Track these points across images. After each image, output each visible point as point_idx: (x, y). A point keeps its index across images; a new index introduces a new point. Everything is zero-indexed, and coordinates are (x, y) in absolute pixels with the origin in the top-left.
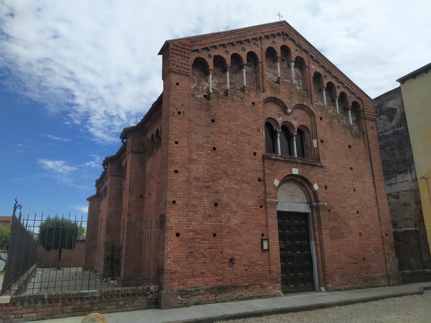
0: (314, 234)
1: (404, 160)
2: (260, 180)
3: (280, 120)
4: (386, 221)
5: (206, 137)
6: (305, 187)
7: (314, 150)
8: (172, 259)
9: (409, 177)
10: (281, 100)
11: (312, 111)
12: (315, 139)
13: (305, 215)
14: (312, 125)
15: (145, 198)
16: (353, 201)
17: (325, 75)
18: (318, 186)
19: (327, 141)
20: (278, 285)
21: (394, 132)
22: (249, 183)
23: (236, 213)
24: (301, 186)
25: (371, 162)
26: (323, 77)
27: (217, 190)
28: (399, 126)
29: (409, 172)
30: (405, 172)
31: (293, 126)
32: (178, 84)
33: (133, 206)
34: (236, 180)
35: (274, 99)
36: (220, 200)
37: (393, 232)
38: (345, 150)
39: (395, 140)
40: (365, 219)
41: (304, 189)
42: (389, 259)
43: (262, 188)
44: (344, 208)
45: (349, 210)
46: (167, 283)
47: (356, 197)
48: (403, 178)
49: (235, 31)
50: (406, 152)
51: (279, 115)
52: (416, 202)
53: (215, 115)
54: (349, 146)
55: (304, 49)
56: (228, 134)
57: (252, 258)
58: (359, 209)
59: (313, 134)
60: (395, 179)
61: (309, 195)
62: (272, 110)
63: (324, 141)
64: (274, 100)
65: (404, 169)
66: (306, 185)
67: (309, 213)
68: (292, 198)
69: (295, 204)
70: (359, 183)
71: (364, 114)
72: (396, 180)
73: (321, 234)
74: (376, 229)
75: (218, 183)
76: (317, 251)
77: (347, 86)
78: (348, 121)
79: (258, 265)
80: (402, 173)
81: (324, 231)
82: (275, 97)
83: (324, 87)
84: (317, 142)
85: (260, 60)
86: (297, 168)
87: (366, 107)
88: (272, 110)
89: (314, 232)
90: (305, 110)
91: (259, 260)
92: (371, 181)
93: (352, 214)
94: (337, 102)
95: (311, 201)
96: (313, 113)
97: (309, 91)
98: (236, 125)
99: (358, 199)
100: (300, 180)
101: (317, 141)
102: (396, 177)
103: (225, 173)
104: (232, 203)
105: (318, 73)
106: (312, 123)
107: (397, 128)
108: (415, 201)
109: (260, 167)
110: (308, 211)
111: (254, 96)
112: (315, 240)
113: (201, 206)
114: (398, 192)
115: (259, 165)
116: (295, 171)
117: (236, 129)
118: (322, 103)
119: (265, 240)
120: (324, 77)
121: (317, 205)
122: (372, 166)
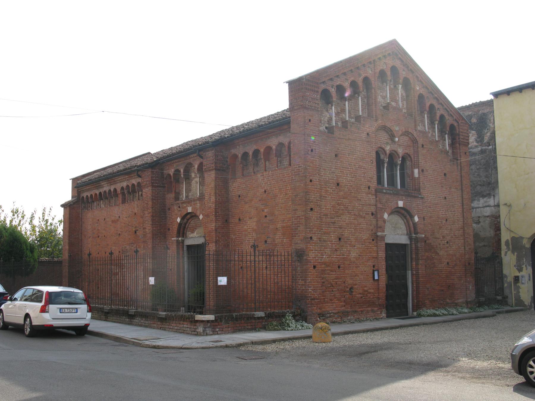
0: (412, 264)
1: (489, 184)
2: (372, 214)
3: (388, 148)
4: (470, 251)
5: (332, 173)
6: (406, 219)
7: (415, 180)
8: (312, 288)
9: (491, 202)
10: (389, 128)
11: (416, 138)
12: (417, 168)
13: (405, 245)
14: (414, 153)
15: (229, 223)
17: (428, 97)
18: (418, 218)
20: (384, 310)
21: (482, 150)
22: (364, 218)
23: (355, 246)
24: (403, 218)
25: (462, 191)
26: (426, 99)
28: (488, 144)
29: (492, 197)
30: (489, 195)
31: (398, 155)
32: (310, 121)
33: (220, 232)
34: (354, 215)
35: (384, 127)
36: (343, 235)
37: (431, 244)
38: (441, 179)
39: (481, 159)
40: (453, 248)
41: (405, 221)
42: (469, 287)
43: (374, 222)
44: (437, 238)
45: (441, 241)
46: (310, 307)
47: (447, 228)
48: (486, 202)
50: (491, 175)
51: (387, 143)
52: (496, 229)
53: (338, 149)
54: (445, 174)
55: (411, 69)
56: (348, 168)
57: (366, 287)
58: (449, 239)
59: (415, 162)
60: (478, 203)
61: (409, 226)
62: (381, 139)
63: (425, 170)
64: (385, 128)
65: (488, 192)
66: (408, 217)
67: (407, 244)
69: (397, 236)
70: (451, 213)
71: (459, 139)
72: (478, 204)
73: (417, 264)
74: (461, 258)
76: (412, 281)
77: (447, 108)
78: (444, 145)
79: (370, 293)
80: (485, 197)
81: (421, 262)
83: (426, 110)
84: (419, 172)
85: (373, 86)
86: (402, 201)
87: (462, 131)
88: (381, 139)
89: (411, 262)
90: (409, 137)
91: (370, 289)
92: (460, 210)
93: (443, 244)
94: (436, 126)
95: (410, 232)
96: (416, 140)
97: (413, 116)
98: (354, 159)
99: (448, 230)
100: (403, 212)
101: (419, 170)
102: (479, 200)
104: (352, 237)
105: (422, 94)
106: (414, 151)
107: (485, 146)
108: (495, 228)
109: (373, 201)
110: (408, 242)
111: (369, 126)
112: (412, 270)
113: (329, 241)
114: (479, 217)
116: (401, 204)
117: (354, 163)
118: (423, 126)
119: (375, 270)
120: (427, 98)
121: (416, 237)
122: (462, 195)
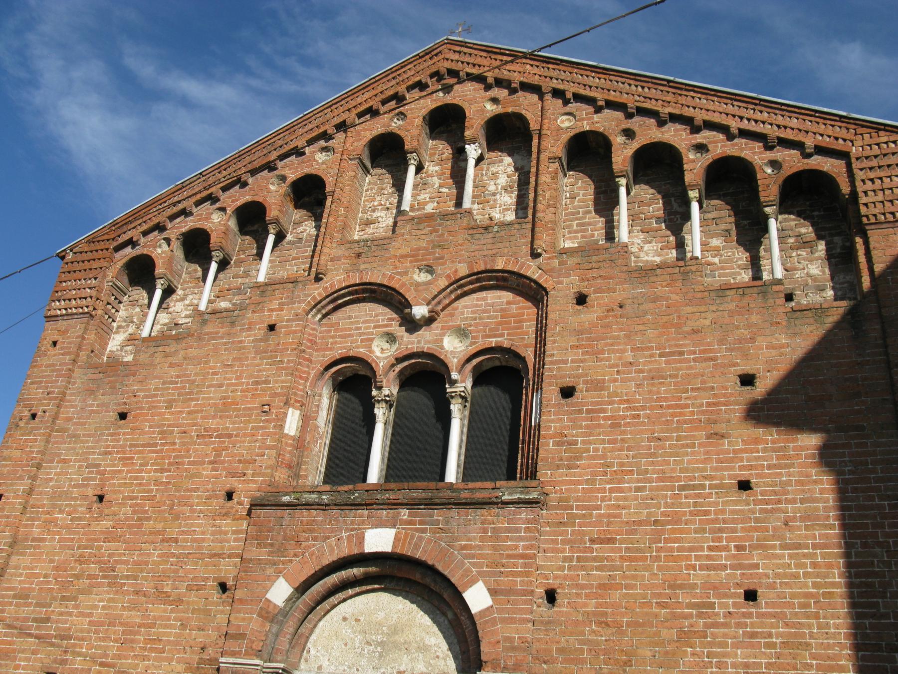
16: (725, 655)
18: (493, 592)
19: (598, 386)
27: (65, 629)
49: (252, 147)
68: (381, 656)
75: (76, 607)
82: (364, 280)
99: (772, 645)
103: (109, 571)
115: (235, 532)
